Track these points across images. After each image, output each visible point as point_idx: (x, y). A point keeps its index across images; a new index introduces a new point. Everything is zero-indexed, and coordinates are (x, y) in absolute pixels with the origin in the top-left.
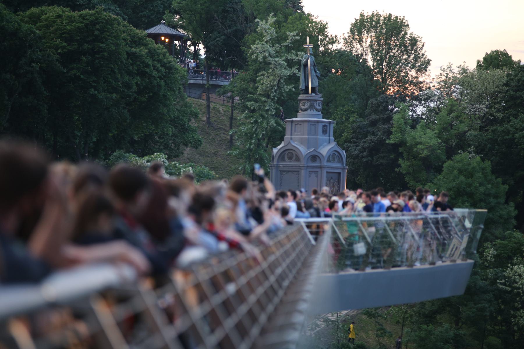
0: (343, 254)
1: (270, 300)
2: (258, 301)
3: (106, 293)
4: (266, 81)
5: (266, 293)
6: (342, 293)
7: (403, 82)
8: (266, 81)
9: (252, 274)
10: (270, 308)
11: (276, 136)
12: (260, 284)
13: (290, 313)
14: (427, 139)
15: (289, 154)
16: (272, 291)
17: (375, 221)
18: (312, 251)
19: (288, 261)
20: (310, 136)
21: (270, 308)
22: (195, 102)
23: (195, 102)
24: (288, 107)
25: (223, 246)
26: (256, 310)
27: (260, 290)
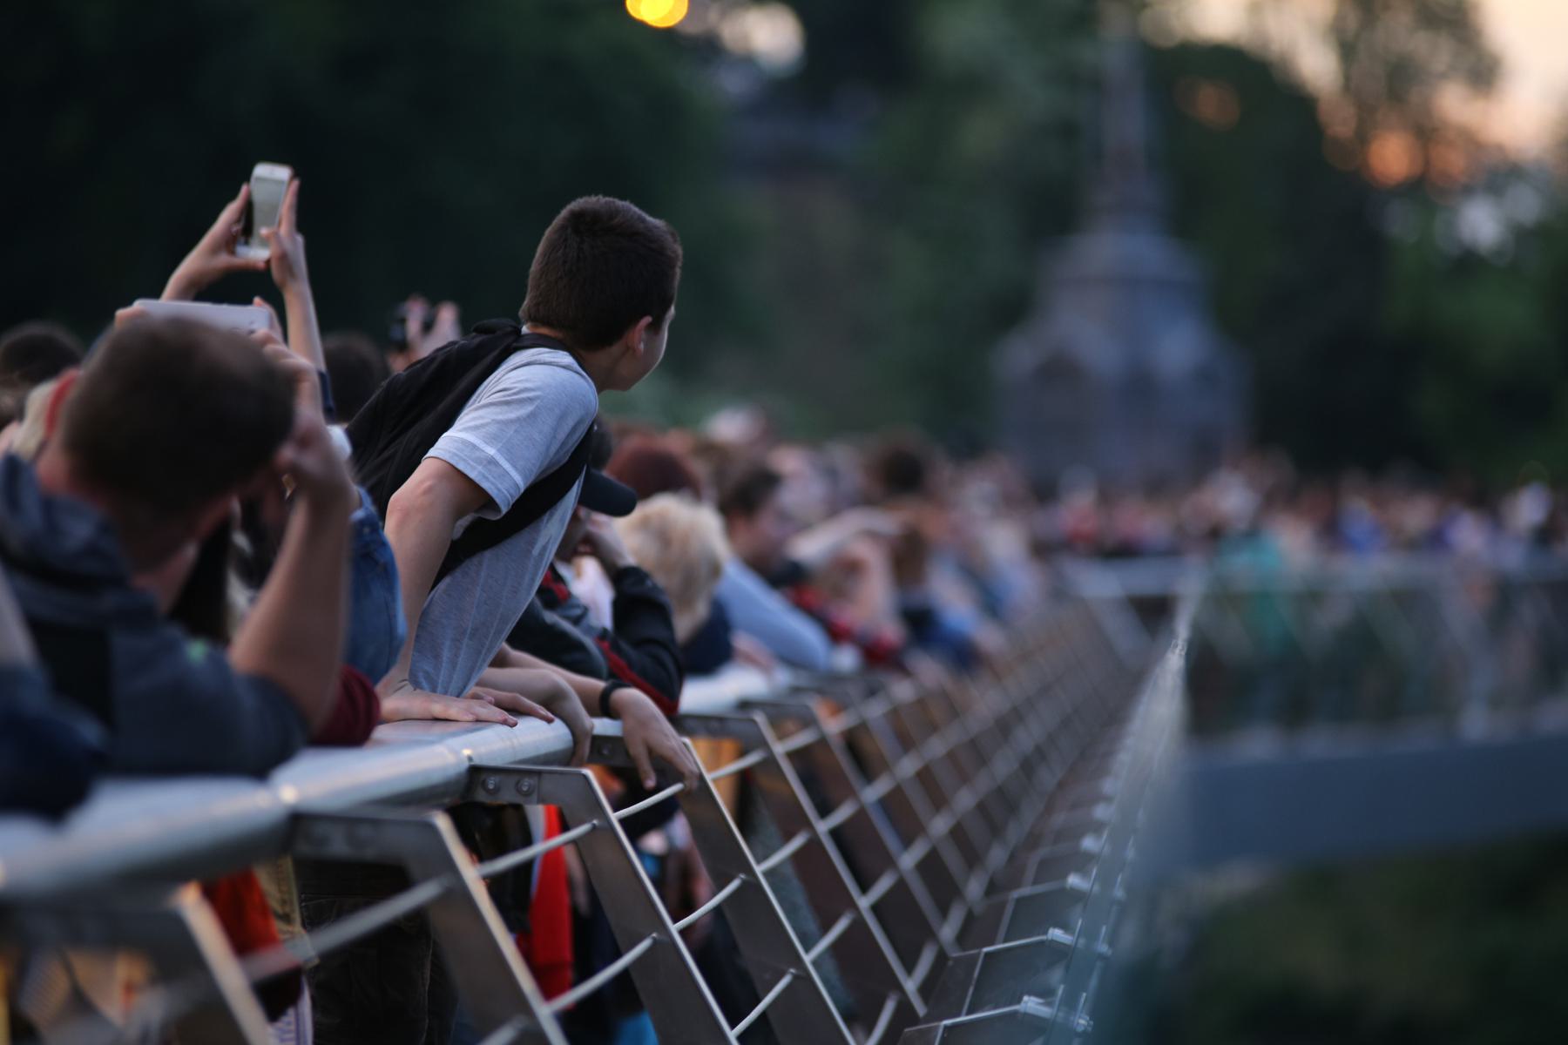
0: (1215, 692)
1: (996, 831)
2: (958, 834)
3: (483, 808)
4: (981, 135)
5: (981, 807)
6: (1213, 813)
7: (1427, 133)
8: (981, 135)
9: (936, 747)
10: (997, 856)
11: (1012, 309)
12: (964, 779)
13: (1053, 868)
14: (1505, 322)
15: (1059, 371)
16: (998, 810)
17: (1172, 634)
18: (1130, 682)
19: (983, 783)
20: (1122, 306)
21: (997, 856)
22: (753, 205)
23: (753, 205)
24: (1052, 212)
25: (846, 659)
26: (952, 859)
27: (965, 800)
